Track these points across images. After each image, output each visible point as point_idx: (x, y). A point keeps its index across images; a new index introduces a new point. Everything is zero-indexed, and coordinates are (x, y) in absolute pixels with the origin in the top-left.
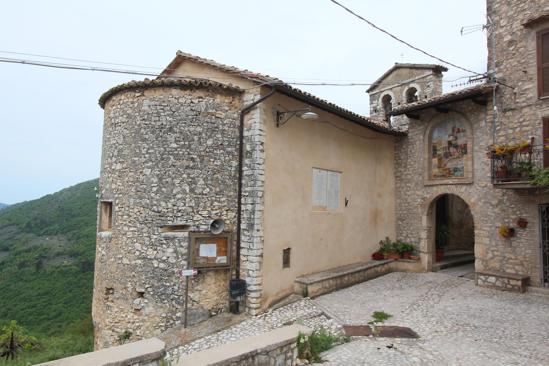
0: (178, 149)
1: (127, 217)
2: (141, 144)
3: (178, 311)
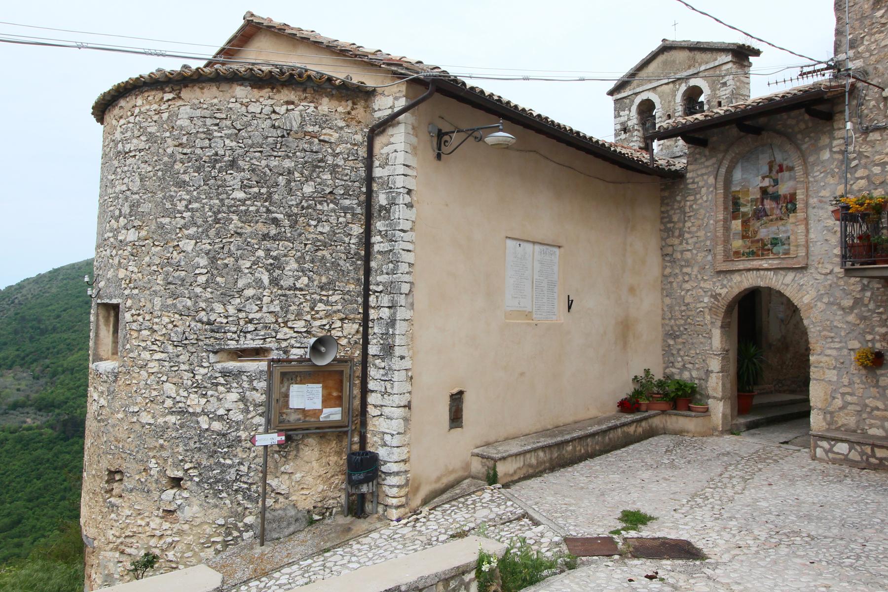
0: (247, 202)
1: (149, 333)
3: (247, 513)
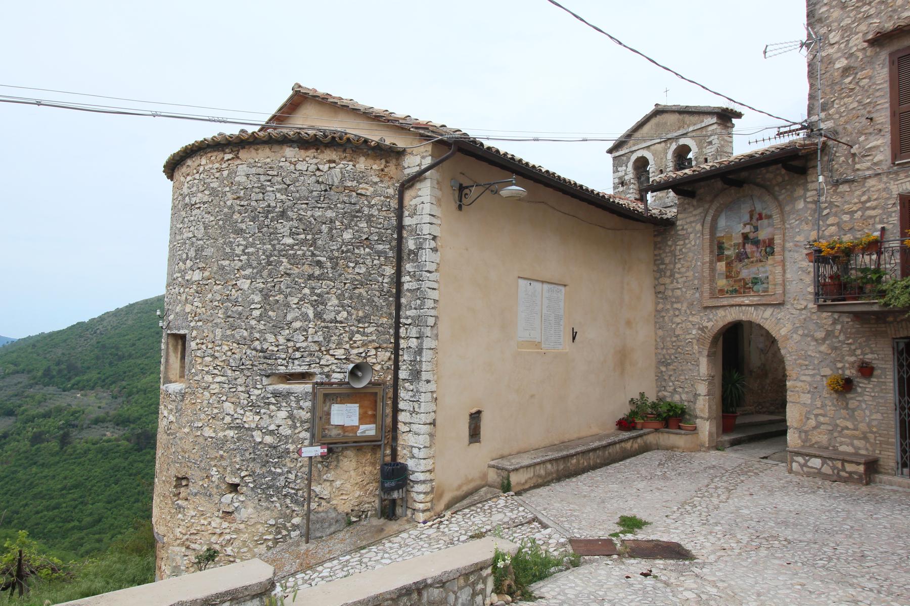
0: (295, 247)
1: (211, 359)
2: (233, 238)
3: (294, 514)
